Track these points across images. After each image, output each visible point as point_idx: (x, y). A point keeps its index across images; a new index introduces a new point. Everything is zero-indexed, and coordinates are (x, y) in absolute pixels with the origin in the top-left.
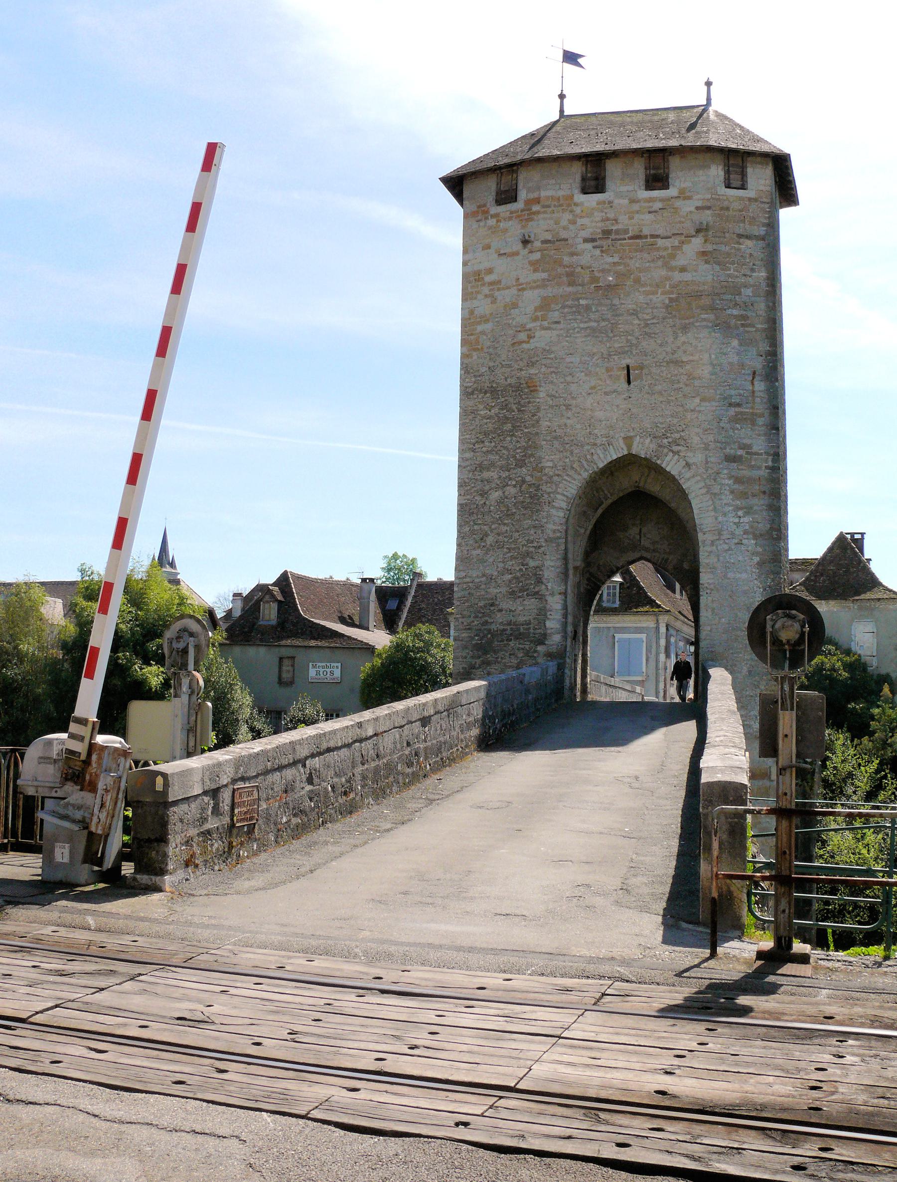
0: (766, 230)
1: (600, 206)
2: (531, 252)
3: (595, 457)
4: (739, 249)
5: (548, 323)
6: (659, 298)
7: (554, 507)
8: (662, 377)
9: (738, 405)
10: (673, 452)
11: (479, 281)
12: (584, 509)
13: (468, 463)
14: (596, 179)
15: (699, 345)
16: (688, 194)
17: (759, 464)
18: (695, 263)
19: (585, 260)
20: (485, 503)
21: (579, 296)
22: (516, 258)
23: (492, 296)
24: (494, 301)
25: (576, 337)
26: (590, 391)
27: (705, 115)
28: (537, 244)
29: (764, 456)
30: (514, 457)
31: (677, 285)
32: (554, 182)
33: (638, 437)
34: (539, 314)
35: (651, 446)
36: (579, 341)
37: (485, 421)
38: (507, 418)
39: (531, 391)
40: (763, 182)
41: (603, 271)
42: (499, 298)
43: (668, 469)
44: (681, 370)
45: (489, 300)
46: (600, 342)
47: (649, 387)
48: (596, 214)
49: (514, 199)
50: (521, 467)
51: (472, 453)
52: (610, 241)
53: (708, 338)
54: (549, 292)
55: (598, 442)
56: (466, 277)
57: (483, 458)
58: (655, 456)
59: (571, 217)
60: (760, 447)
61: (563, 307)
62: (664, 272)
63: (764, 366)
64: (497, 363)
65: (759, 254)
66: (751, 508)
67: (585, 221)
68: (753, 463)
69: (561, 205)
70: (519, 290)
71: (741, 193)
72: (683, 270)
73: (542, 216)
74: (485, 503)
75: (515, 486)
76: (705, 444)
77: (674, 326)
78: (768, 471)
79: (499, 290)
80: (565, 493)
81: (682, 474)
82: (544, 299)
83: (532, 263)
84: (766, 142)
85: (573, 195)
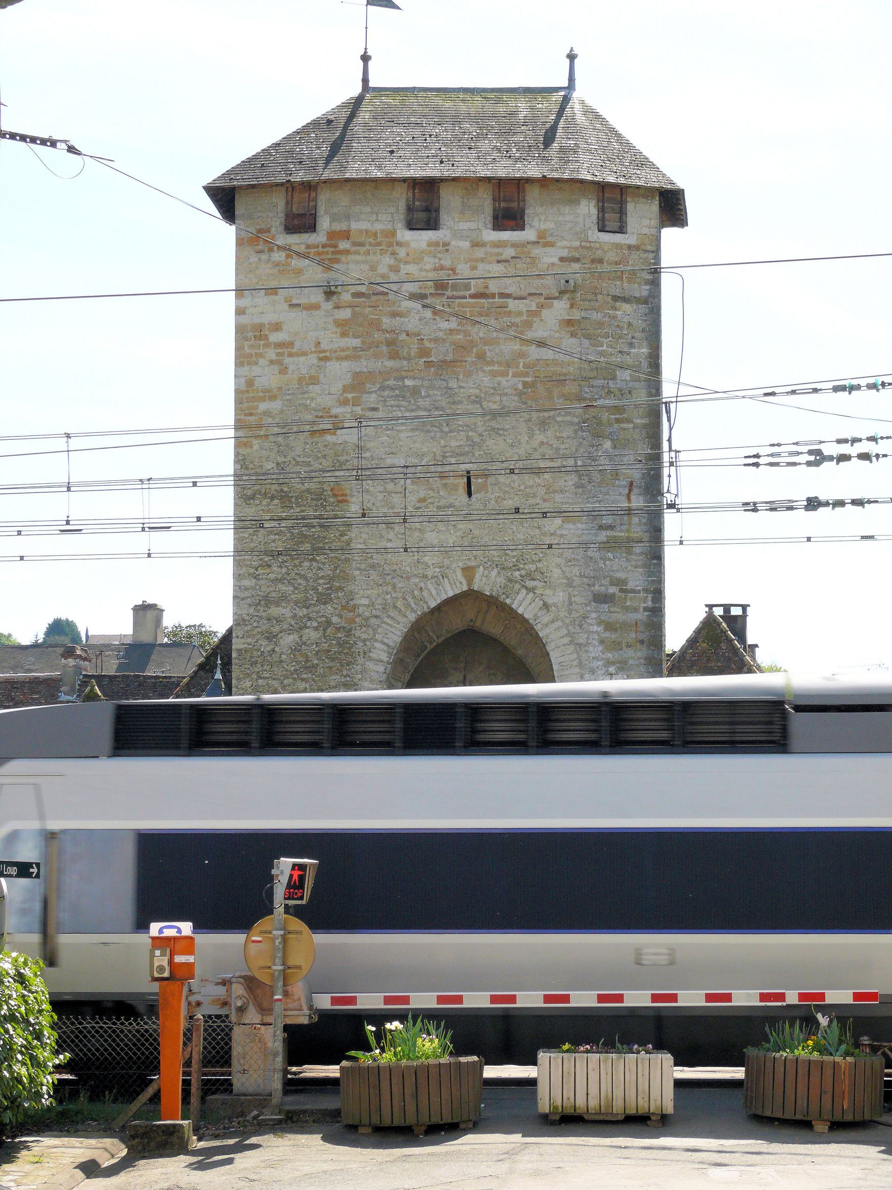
0: (650, 290)
1: (432, 249)
2: (337, 307)
3: (425, 593)
4: (614, 317)
5: (362, 409)
6: (509, 382)
7: (370, 659)
8: (513, 488)
9: (611, 527)
10: (526, 588)
11: (260, 340)
12: (401, 655)
13: (247, 594)
14: (427, 210)
15: (563, 447)
16: (549, 239)
17: (636, 604)
18: (557, 335)
19: (412, 323)
20: (273, 650)
21: (404, 374)
22: (315, 313)
23: (280, 363)
24: (284, 370)
25: (400, 431)
26: (418, 505)
27: (568, 110)
28: (346, 297)
29: (642, 595)
30: (315, 589)
31: (534, 365)
32: (368, 209)
33: (481, 567)
34: (350, 396)
35: (499, 580)
36: (403, 435)
37: (273, 537)
38: (306, 536)
39: (339, 501)
40: (646, 222)
41: (436, 340)
42: (292, 367)
43: (520, 611)
44: (537, 480)
45: (276, 368)
46: (432, 438)
47: (496, 501)
48: (426, 259)
49: (312, 228)
50: (325, 603)
51: (254, 581)
52: (444, 299)
53: (574, 438)
54: (364, 365)
55: (430, 573)
56: (240, 330)
57: (271, 589)
58: (504, 593)
59: (392, 262)
60: (638, 583)
61: (383, 388)
62: (516, 346)
63: (643, 474)
64: (289, 458)
65: (640, 323)
66: (626, 662)
67: (412, 269)
68: (628, 603)
69: (379, 244)
70: (320, 359)
71: (618, 238)
72: (541, 344)
73: (351, 257)
74: (273, 650)
75: (316, 629)
76: (568, 579)
77: (530, 420)
78: (646, 613)
79: (290, 355)
80: (386, 640)
81: (539, 618)
82: (356, 375)
83: (338, 323)
84: (653, 166)
85: (395, 231)
